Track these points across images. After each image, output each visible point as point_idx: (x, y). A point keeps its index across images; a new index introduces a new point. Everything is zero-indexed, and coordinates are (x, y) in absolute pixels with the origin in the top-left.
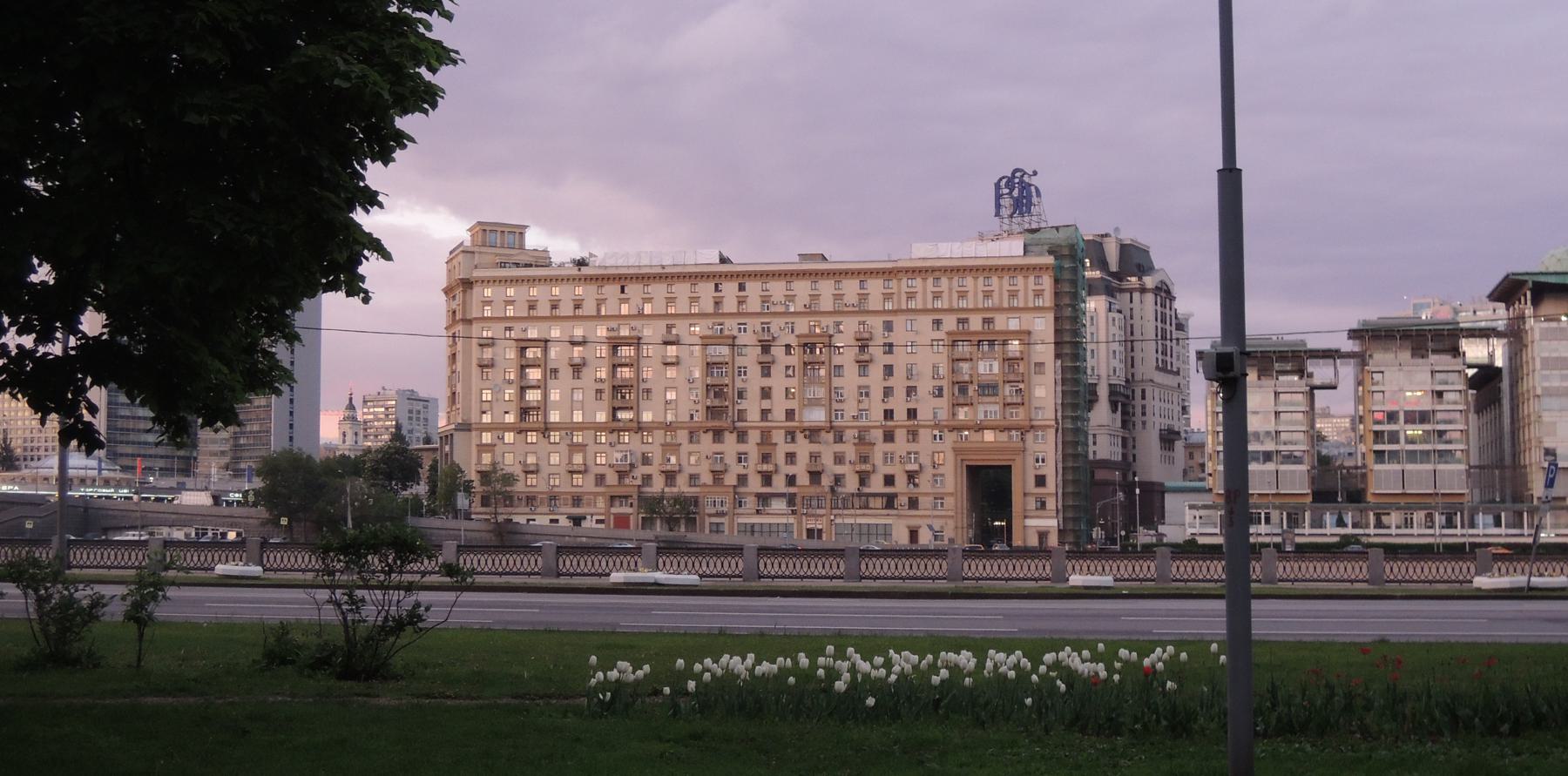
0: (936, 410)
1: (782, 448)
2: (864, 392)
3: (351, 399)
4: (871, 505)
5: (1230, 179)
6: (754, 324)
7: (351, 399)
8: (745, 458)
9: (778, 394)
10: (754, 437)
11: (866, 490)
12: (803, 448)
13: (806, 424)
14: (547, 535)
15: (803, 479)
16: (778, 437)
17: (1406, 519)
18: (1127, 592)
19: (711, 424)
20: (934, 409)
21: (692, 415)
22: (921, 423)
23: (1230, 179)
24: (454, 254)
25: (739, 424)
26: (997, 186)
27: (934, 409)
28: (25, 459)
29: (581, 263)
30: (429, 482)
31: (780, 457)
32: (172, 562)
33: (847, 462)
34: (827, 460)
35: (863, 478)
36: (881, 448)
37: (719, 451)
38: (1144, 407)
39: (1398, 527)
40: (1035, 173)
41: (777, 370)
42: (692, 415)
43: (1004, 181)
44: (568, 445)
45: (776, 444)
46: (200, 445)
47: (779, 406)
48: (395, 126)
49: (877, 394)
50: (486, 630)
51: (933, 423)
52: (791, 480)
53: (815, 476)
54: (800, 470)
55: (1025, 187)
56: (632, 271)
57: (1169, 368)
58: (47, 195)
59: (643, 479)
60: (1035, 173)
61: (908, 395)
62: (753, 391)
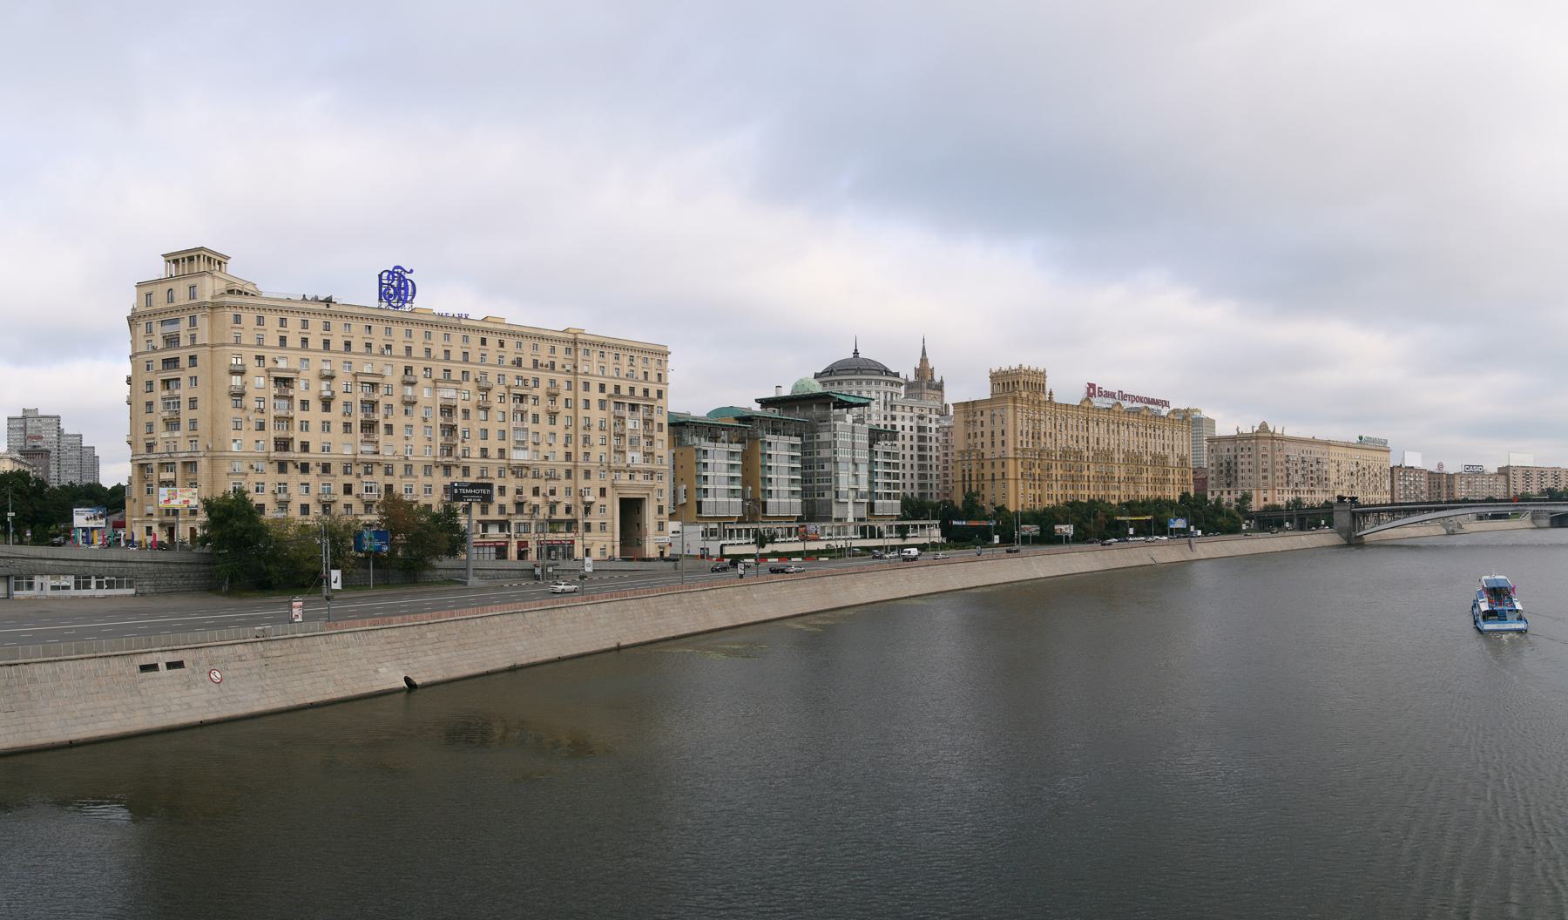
3: (924, 353)
5: (924, 349)
7: (924, 353)
11: (554, 517)
15: (511, 509)
23: (924, 349)
24: (174, 316)
26: (380, 276)
29: (328, 301)
30: (207, 507)
34: (527, 495)
38: (154, 667)
39: (782, 537)
40: (411, 271)
41: (495, 414)
43: (387, 274)
47: (493, 445)
49: (561, 439)
53: (519, 506)
55: (402, 279)
56: (533, 331)
60: (411, 271)
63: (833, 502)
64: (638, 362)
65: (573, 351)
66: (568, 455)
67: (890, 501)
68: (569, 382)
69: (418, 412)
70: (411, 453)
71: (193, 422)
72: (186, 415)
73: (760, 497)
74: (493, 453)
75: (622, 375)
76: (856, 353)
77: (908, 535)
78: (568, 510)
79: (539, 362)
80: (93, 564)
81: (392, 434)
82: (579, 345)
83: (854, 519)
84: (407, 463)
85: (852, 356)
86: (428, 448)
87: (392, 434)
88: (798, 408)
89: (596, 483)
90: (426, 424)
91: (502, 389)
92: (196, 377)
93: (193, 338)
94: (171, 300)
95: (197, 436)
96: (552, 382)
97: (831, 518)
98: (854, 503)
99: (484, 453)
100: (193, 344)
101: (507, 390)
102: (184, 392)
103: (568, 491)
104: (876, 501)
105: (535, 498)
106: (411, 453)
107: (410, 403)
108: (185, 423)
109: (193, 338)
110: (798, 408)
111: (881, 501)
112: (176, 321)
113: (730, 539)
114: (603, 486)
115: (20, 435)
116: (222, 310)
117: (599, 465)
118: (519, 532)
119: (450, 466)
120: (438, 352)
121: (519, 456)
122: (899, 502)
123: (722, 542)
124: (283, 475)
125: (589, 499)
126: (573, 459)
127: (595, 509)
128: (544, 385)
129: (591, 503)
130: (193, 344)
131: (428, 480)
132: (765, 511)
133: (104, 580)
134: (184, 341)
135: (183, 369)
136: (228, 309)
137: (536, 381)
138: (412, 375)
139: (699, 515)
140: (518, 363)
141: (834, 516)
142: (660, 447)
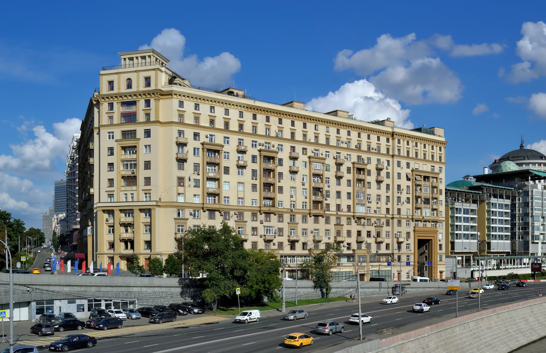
1: (345, 228)
2: (379, 197)
4: (381, 260)
6: (333, 152)
9: (344, 195)
10: (333, 220)
11: (380, 252)
12: (354, 228)
13: (357, 214)
14: (334, 345)
15: (354, 246)
16: (344, 221)
17: (407, 246)
18: (94, 215)
22: (402, 216)
24: (130, 99)
25: (327, 212)
31: (344, 233)
33: (372, 237)
36: (385, 229)
37: (317, 228)
44: (235, 221)
45: (298, 224)
47: (345, 202)
49: (384, 199)
50: (157, 330)
51: (406, 217)
53: (359, 243)
57: (211, 203)
58: (180, 311)
59: (278, 245)
62: (333, 194)
63: (530, 242)
64: (205, 109)
65: (390, 139)
66: (388, 210)
67: (468, 241)
68: (388, 161)
69: (298, 177)
70: (294, 207)
71: (148, 181)
72: (142, 174)
73: (486, 239)
74: (344, 208)
75: (273, 134)
76: (521, 146)
77: (501, 267)
78: (387, 246)
79: (371, 147)
80: (103, 289)
81: (282, 193)
82: (395, 136)
83: (542, 253)
84: (293, 214)
85: (519, 148)
86: (304, 204)
87: (282, 193)
88: (504, 180)
89: (404, 229)
90: (304, 187)
91: (198, 144)
92: (150, 146)
93: (148, 115)
94: (129, 86)
95: (150, 190)
96: (379, 160)
97: (529, 253)
98: (542, 243)
99: (338, 207)
100: (148, 121)
101: (352, 165)
102: (142, 156)
103: (388, 235)
104: (492, 241)
105: (368, 239)
106: (294, 207)
107: (294, 172)
108: (141, 181)
109: (148, 115)
110: (504, 180)
111: (460, 241)
112: (134, 103)
113: (514, 265)
114: (408, 231)
115: (304, 204)
116: (171, 96)
117: (406, 217)
118: (360, 262)
119: (318, 216)
120: (311, 137)
121: (361, 210)
122: (476, 241)
123: (472, 269)
124: (317, 225)
125: (401, 240)
126: (352, 211)
127: (403, 246)
128: (374, 162)
129: (402, 243)
130: (148, 121)
131: (305, 226)
132: (489, 248)
133: (112, 302)
134: (141, 117)
135: (139, 139)
136: (175, 96)
137: (369, 159)
138: (243, 146)
139: (452, 251)
140: (358, 148)
141: (531, 252)
142: (227, 188)
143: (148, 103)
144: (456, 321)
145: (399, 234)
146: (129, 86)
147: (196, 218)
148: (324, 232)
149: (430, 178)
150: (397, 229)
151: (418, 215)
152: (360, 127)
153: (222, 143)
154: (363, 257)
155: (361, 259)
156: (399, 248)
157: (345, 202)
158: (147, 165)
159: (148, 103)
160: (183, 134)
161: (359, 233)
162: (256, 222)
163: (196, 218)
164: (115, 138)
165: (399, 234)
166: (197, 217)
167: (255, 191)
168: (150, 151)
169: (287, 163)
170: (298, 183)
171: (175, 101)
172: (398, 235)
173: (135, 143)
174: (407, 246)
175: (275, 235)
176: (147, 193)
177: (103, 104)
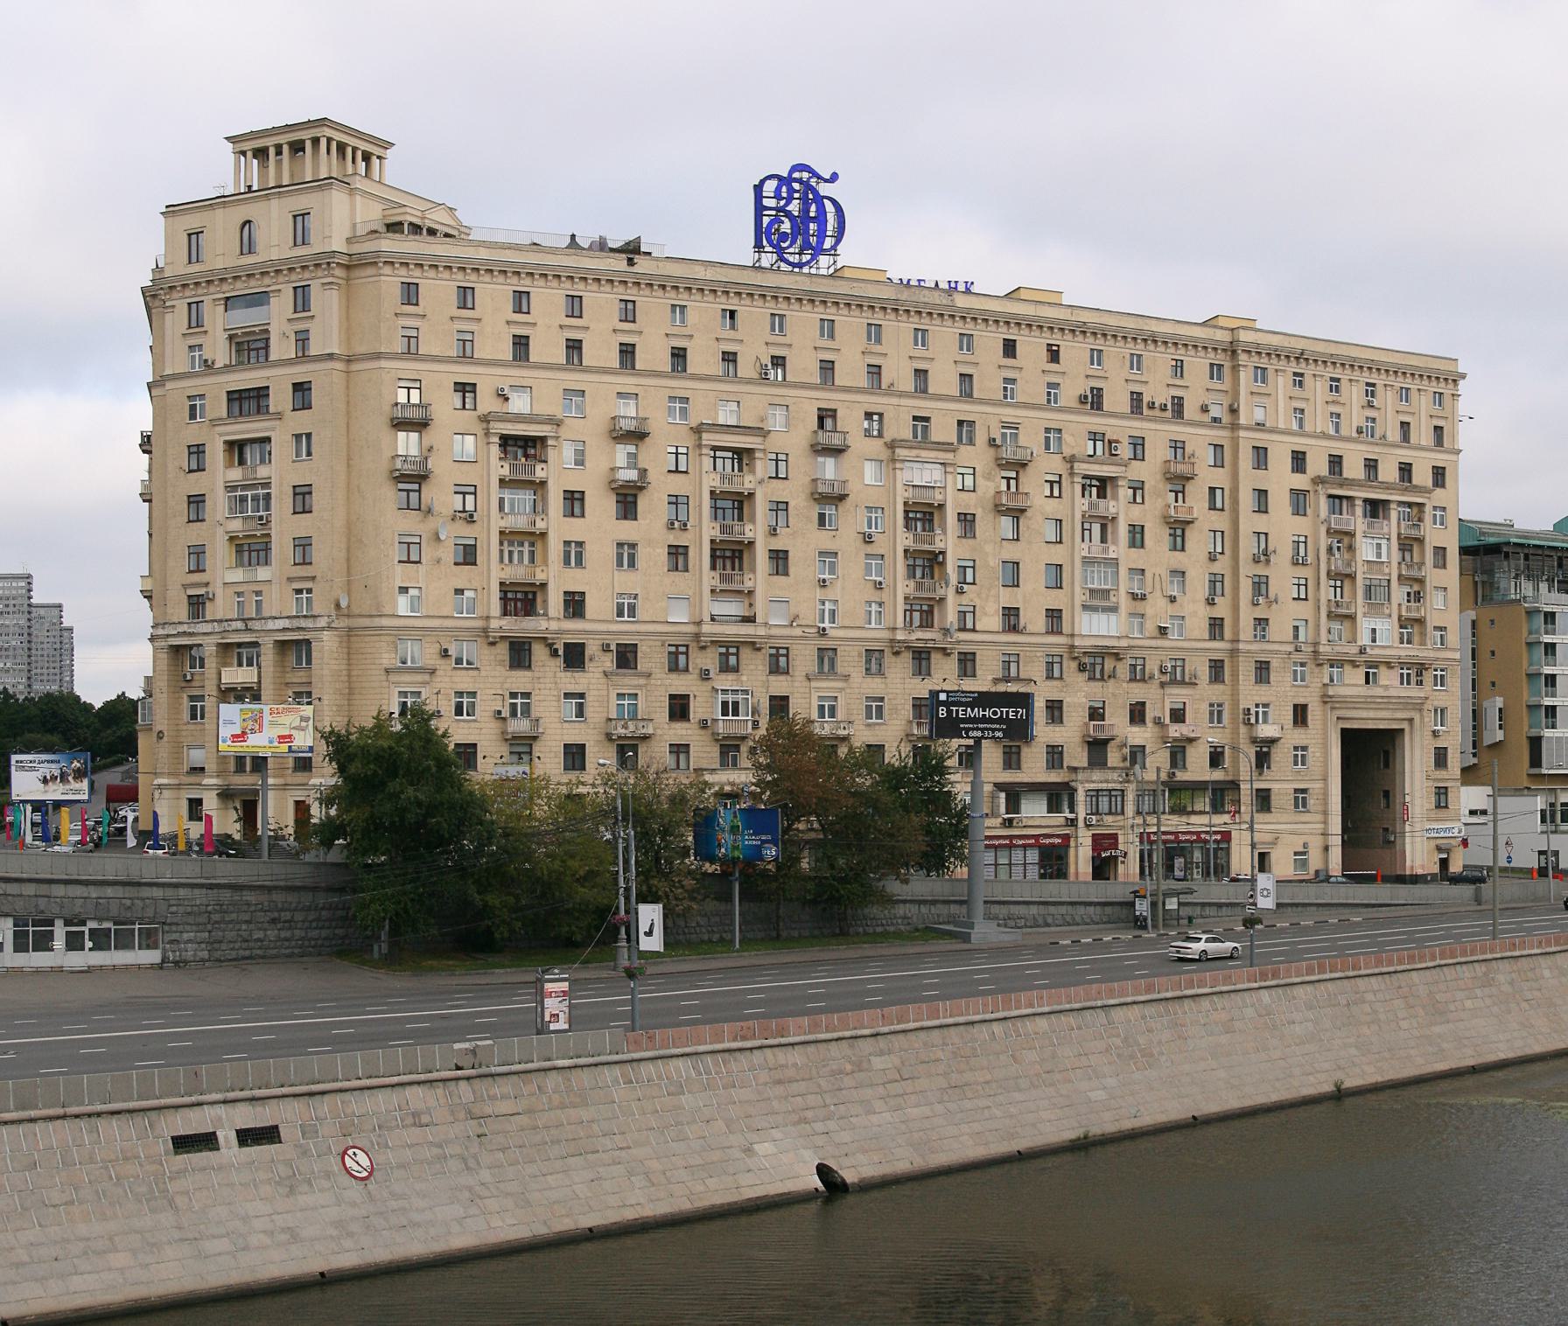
0: (876, 417)
8: (879, 708)
9: (600, 552)
11: (1181, 776)
15: (1077, 756)
19: (1406, 651)
20: (881, 415)
21: (1296, 628)
24: (255, 286)
27: (881, 415)
28: (29, 642)
32: (1234, 816)
35: (1178, 753)
42: (1296, 628)
46: (166, 656)
47: (1033, 600)
48: (88, 707)
52: (1055, 755)
53: (1097, 747)
54: (1070, 734)
61: (432, 447)
66: (1216, 626)
69: (851, 520)
72: (284, 526)
74: (1034, 619)
78: (1216, 759)
82: (1243, 357)
86: (874, 607)
89: (1283, 692)
90: (870, 549)
91: (1055, 465)
92: (309, 436)
93: (302, 339)
94: (248, 247)
96: (1177, 446)
100: (303, 356)
103: (1216, 713)
105: (1135, 729)
108: (281, 547)
109: (302, 339)
112: (260, 299)
114: (1301, 701)
121: (1095, 628)
125: (1266, 731)
127: (1281, 757)
128: (1157, 452)
129: (1272, 741)
130: (303, 356)
131: (875, 686)
134: (282, 348)
135: (279, 416)
136: (387, 270)
137: (1138, 444)
140: (1094, 401)
143: (302, 299)
144: (593, 706)
145: (1261, 710)
146: (248, 247)
147: (465, 665)
148: (1292, 796)
149: (1393, 506)
150: (1251, 694)
151: (1332, 641)
152: (1095, 328)
153: (558, 412)
154: (1110, 796)
155: (1104, 803)
156: (1262, 760)
157: (1033, 600)
158: (302, 497)
159: (302, 299)
160: (472, 395)
161: (1096, 714)
162: (683, 676)
163: (465, 665)
164: (210, 414)
165: (1261, 710)
166: (468, 663)
167: (680, 566)
168: (309, 454)
169: (1159, 500)
170: (845, 538)
171: (390, 282)
172: (1257, 713)
173: (267, 429)
174: (1296, 756)
175: (757, 718)
176: (624, 694)
177: (173, 306)
